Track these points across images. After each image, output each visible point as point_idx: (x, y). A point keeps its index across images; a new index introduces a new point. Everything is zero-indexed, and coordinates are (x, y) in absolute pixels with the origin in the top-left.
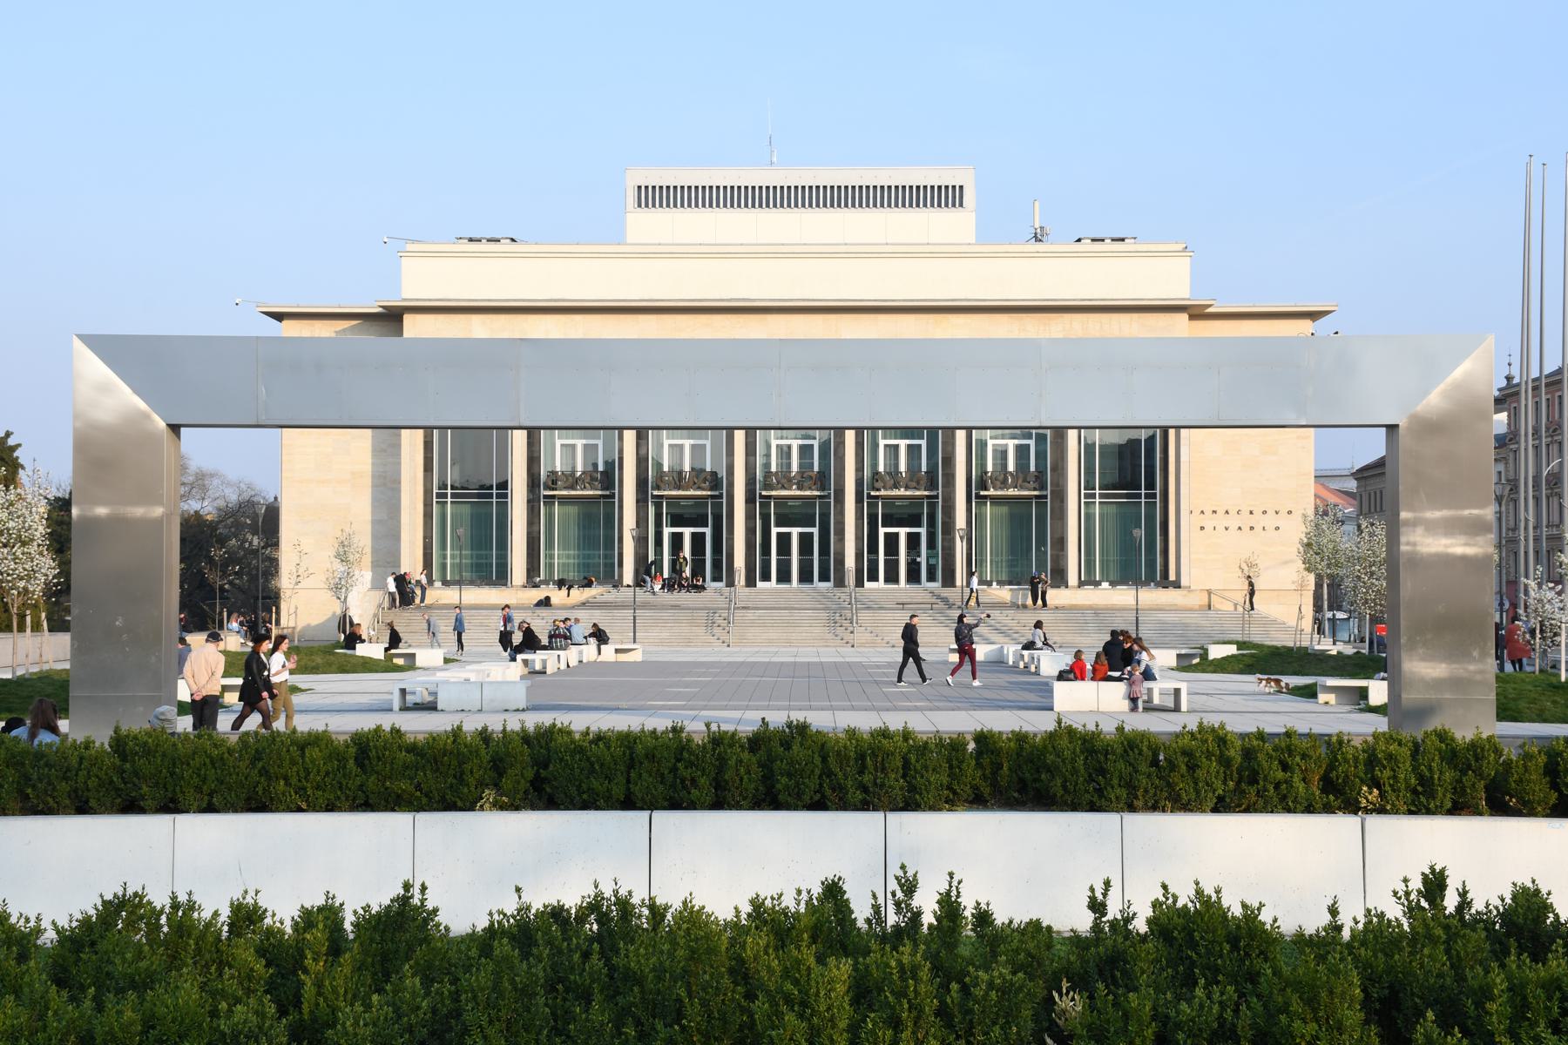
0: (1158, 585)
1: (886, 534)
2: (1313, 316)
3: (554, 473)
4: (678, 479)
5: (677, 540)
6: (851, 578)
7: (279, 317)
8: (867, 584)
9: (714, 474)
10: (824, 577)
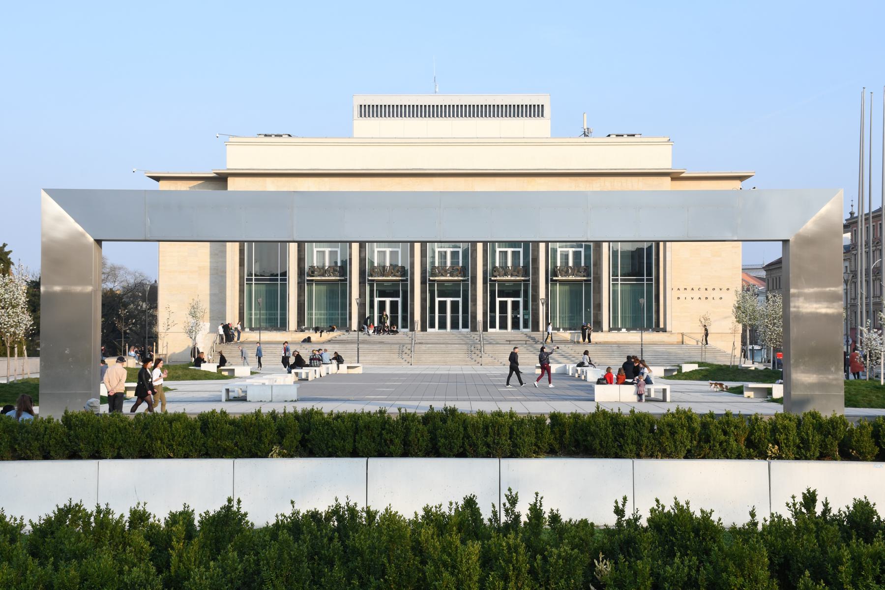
0: (653, 330)
1: (500, 302)
2: (741, 178)
3: (313, 267)
4: (383, 271)
5: (382, 305)
6: (480, 326)
7: (157, 179)
8: (490, 330)
9: (403, 267)
10: (465, 326)
